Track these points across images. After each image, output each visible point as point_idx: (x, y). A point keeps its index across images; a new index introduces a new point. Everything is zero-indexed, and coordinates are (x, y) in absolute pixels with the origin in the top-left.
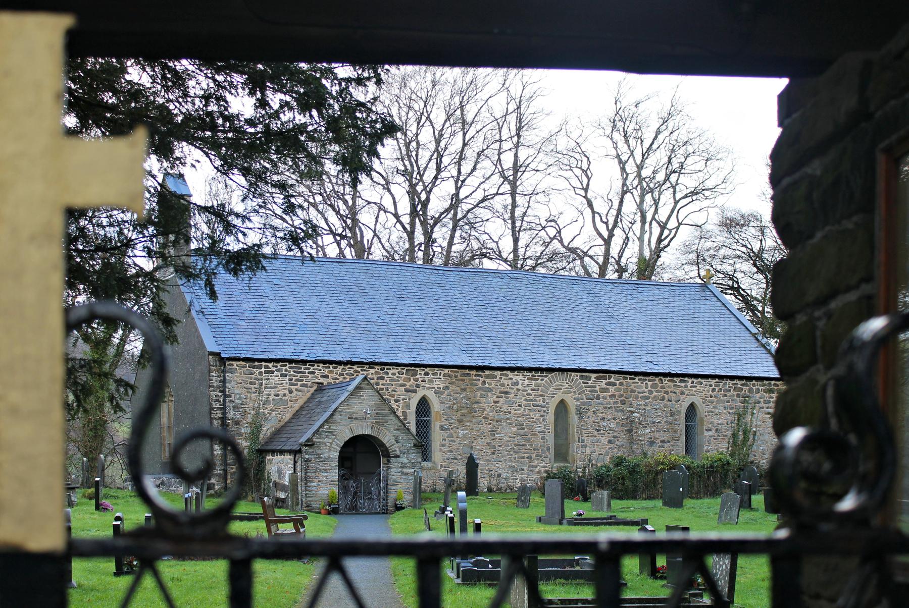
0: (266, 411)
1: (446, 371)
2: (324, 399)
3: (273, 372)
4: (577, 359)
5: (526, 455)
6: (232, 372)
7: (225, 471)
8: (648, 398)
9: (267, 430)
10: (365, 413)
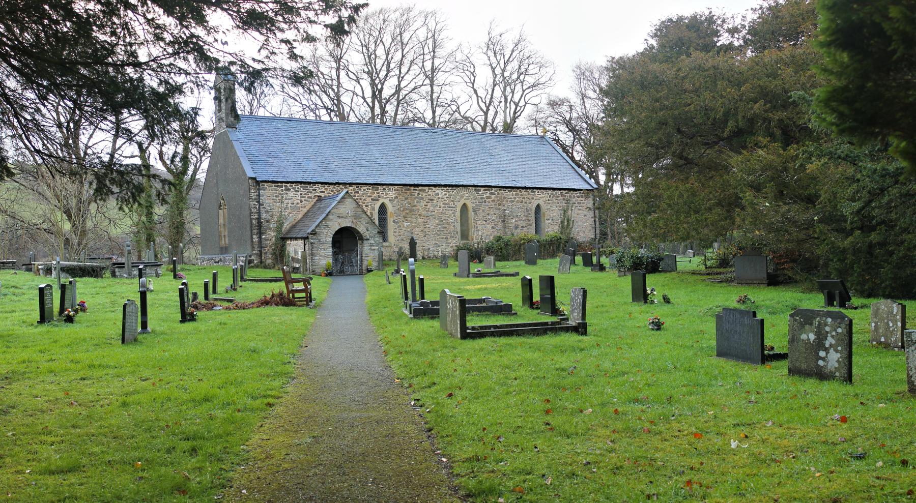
4: (473, 180)
7: (261, 252)
9: (287, 225)
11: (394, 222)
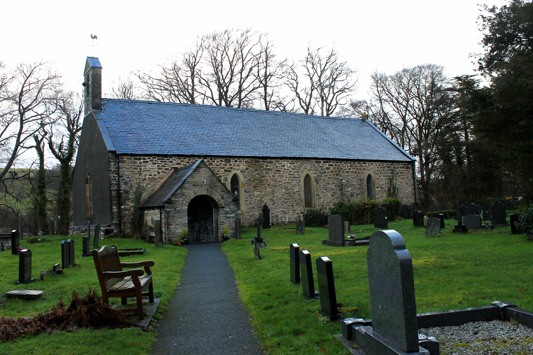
0: (144, 185)
1: (247, 160)
2: (178, 175)
3: (148, 162)
4: (313, 153)
5: (291, 204)
6: (124, 162)
7: (120, 221)
8: (348, 172)
9: (145, 196)
10: (203, 182)
11: (245, 191)
